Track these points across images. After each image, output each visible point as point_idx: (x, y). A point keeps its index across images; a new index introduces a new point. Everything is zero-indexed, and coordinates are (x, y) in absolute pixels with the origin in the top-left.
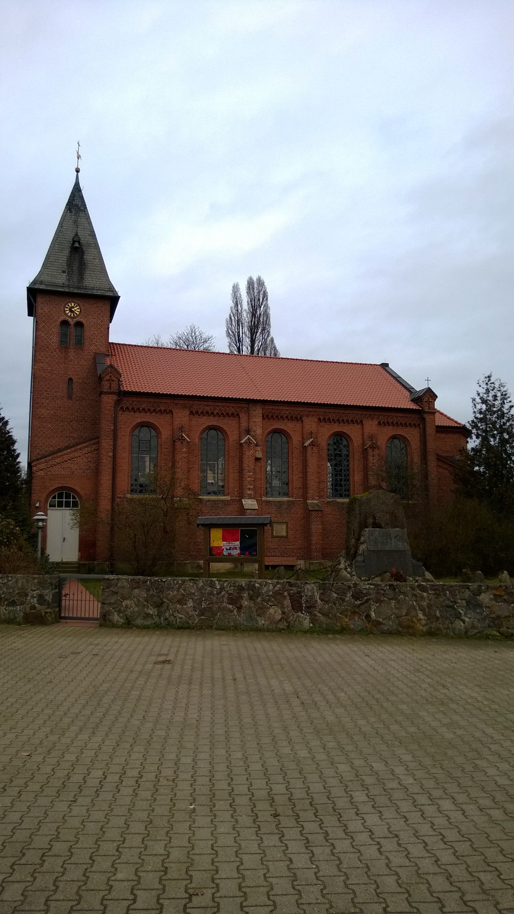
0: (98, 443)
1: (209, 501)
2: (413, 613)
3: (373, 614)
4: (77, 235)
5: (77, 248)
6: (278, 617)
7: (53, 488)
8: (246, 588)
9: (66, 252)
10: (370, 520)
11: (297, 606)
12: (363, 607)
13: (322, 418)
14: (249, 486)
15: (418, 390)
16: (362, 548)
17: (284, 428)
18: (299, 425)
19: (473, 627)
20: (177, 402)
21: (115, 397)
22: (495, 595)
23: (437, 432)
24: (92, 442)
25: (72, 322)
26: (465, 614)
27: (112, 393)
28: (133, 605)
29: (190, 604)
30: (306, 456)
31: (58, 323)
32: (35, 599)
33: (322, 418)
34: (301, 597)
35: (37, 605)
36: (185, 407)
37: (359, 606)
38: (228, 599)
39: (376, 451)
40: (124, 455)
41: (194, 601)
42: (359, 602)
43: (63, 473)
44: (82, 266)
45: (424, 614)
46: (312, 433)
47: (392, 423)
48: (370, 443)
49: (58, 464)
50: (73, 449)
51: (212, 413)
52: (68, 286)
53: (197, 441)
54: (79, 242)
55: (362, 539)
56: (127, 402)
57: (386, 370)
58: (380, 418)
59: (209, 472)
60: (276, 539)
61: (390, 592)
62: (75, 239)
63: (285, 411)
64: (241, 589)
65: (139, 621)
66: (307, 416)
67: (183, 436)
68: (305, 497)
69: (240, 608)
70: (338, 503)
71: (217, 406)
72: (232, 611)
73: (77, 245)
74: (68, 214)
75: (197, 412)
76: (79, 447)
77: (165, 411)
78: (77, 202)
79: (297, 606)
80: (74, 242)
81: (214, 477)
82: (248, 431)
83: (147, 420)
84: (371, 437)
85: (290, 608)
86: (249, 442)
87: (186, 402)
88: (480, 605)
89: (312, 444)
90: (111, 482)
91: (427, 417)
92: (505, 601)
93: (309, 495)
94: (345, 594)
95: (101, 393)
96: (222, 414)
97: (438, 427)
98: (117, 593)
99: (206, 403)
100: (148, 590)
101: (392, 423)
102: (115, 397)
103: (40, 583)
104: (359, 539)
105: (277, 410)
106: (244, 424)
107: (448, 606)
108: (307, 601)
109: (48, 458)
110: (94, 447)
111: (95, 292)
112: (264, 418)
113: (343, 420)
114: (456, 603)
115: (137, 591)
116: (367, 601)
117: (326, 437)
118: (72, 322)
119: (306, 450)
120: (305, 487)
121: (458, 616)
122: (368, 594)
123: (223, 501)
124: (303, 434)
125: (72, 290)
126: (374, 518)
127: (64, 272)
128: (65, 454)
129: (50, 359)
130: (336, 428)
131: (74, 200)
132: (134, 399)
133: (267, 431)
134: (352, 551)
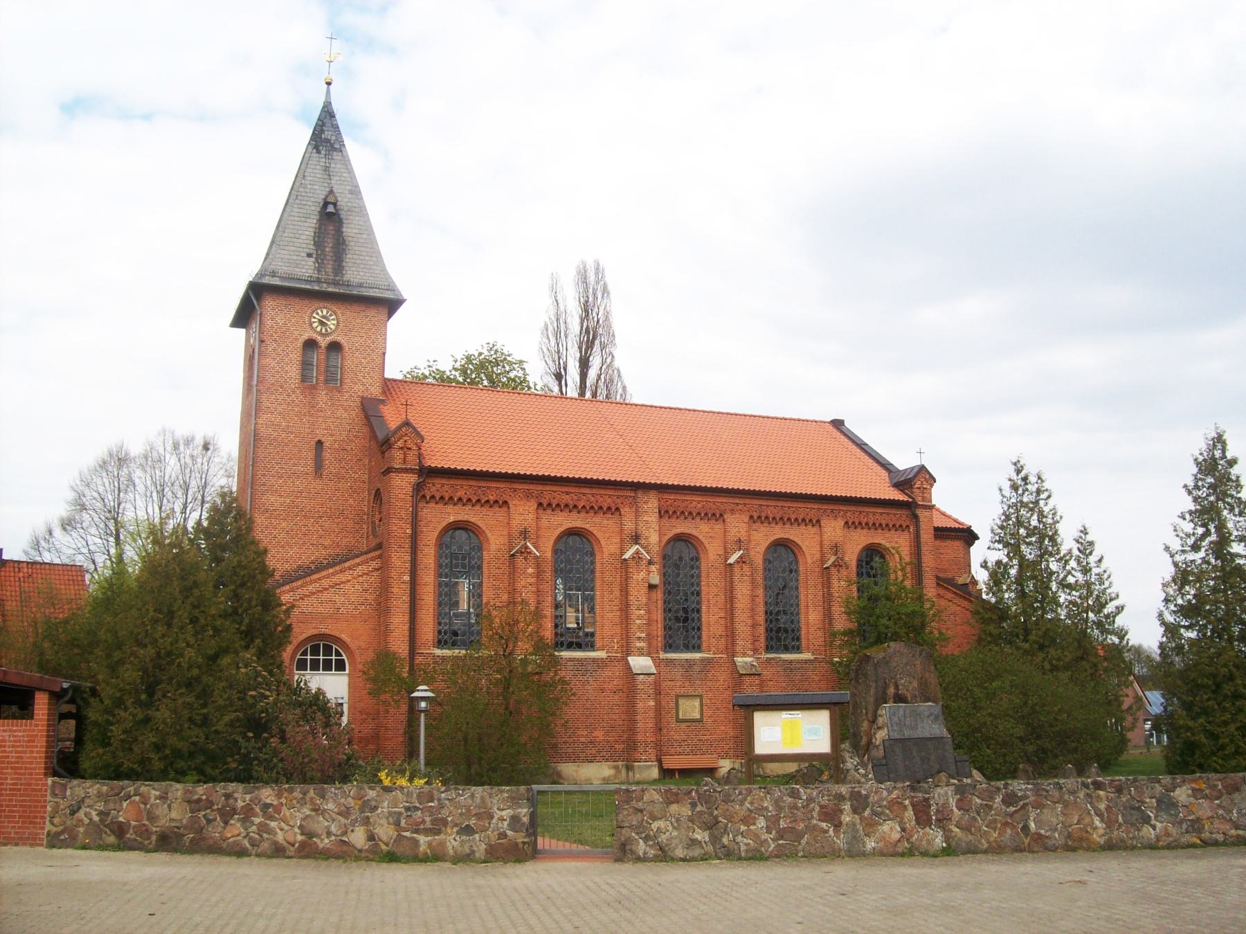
0: (380, 557)
1: (571, 660)
2: (1087, 820)
3: (1032, 825)
4: (331, 192)
5: (330, 215)
6: (896, 836)
7: (305, 636)
8: (847, 796)
9: (313, 221)
10: (891, 690)
11: (923, 818)
12: (1017, 816)
13: (755, 515)
14: (638, 634)
15: (901, 468)
16: (881, 735)
17: (694, 532)
18: (718, 527)
19: (1168, 834)
20: (515, 486)
21: (413, 478)
22: (1193, 789)
23: (936, 537)
24: (369, 556)
25: (323, 342)
26: (1156, 817)
27: (406, 471)
28: (670, 828)
29: (761, 823)
30: (732, 582)
31: (300, 344)
32: (506, 823)
33: (755, 515)
34: (930, 806)
35: (509, 833)
36: (528, 495)
37: (1012, 815)
38: (820, 813)
39: (844, 573)
40: (428, 579)
41: (767, 819)
42: (1012, 809)
43: (321, 609)
44: (340, 247)
45: (1102, 821)
46: (740, 541)
47: (867, 524)
48: (833, 559)
49: (313, 593)
50: (337, 568)
51: (575, 506)
52: (319, 281)
53: (549, 554)
54: (335, 204)
55: (880, 721)
56: (436, 487)
57: (842, 432)
58: (849, 514)
59: (569, 609)
60: (683, 725)
61: (1056, 794)
62: (329, 200)
63: (696, 502)
64: (840, 797)
65: (679, 853)
66: (732, 511)
67: (527, 548)
68: (731, 652)
69: (837, 826)
70: (785, 661)
71: (584, 494)
72: (827, 832)
73: (331, 209)
74: (315, 155)
75: (549, 505)
76: (347, 564)
77: (496, 502)
78: (327, 134)
79: (923, 818)
80: (326, 204)
81: (577, 618)
82: (636, 539)
83: (466, 518)
84: (836, 548)
85: (913, 823)
86: (637, 557)
87: (531, 487)
88: (1173, 805)
89: (741, 561)
90: (407, 627)
91: (922, 514)
92: (1206, 797)
93: (738, 648)
94: (992, 798)
95: (389, 471)
96: (592, 508)
97: (937, 529)
98: (641, 811)
99: (566, 489)
100: (694, 805)
101: (867, 524)
102: (413, 478)
103: (512, 798)
104: (874, 721)
105: (683, 501)
106: (629, 526)
107: (1133, 808)
108: (938, 811)
109: (295, 584)
110: (374, 564)
111: (365, 292)
112: (661, 517)
113: (789, 519)
114: (1143, 802)
115: (674, 808)
116: (1024, 807)
117: (762, 548)
118: (323, 342)
119: (732, 571)
120: (731, 635)
121: (1147, 820)
122: (1026, 797)
123: (594, 660)
124: (725, 542)
125: (324, 287)
126: (897, 687)
127: (309, 255)
128: (324, 577)
129: (284, 406)
130: (779, 532)
131: (322, 131)
132: (444, 481)
133: (667, 538)
134: (864, 741)
